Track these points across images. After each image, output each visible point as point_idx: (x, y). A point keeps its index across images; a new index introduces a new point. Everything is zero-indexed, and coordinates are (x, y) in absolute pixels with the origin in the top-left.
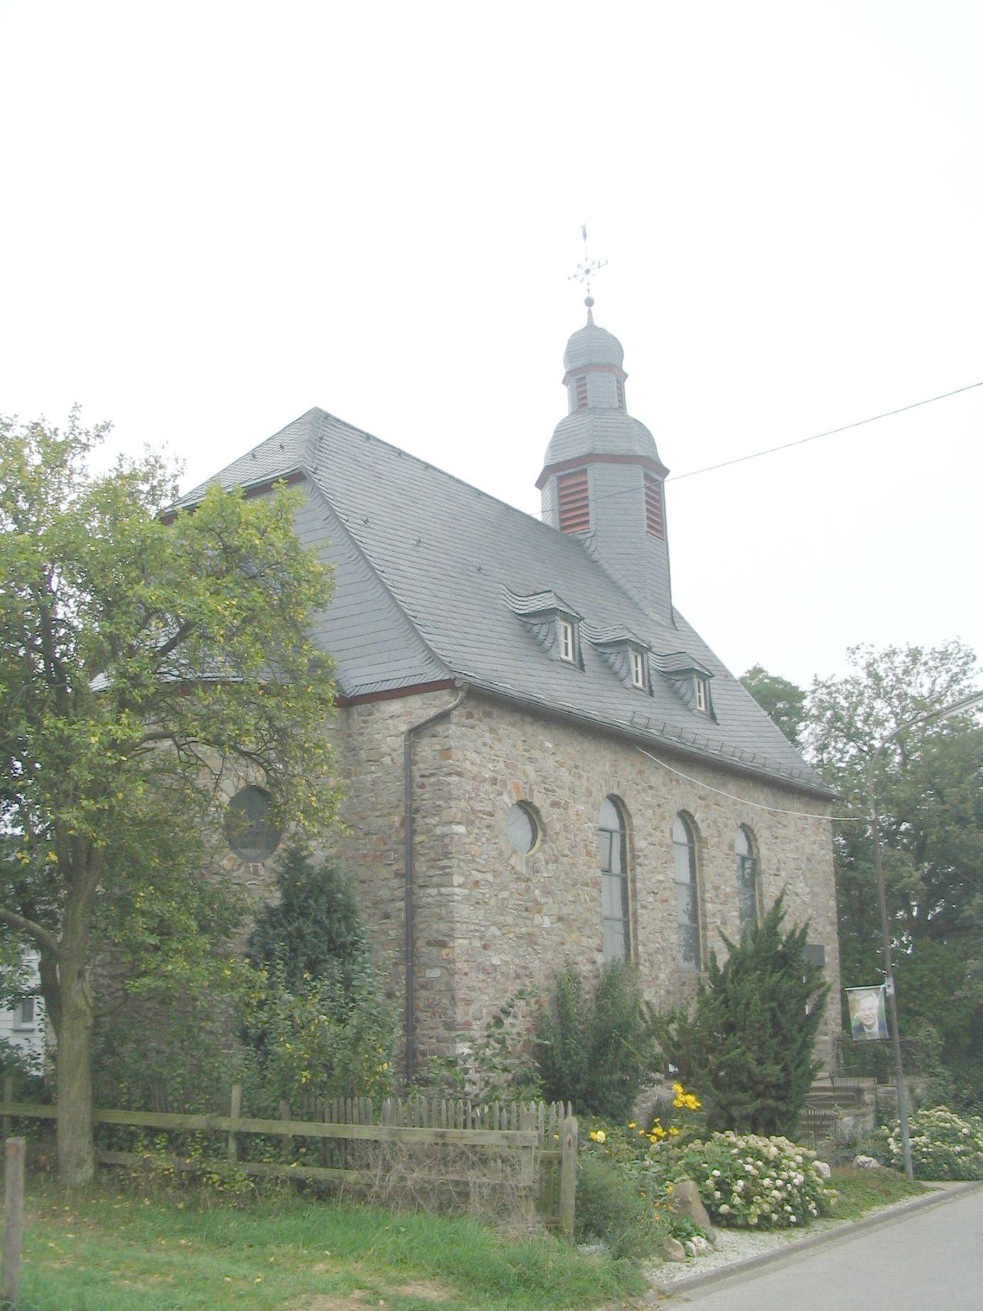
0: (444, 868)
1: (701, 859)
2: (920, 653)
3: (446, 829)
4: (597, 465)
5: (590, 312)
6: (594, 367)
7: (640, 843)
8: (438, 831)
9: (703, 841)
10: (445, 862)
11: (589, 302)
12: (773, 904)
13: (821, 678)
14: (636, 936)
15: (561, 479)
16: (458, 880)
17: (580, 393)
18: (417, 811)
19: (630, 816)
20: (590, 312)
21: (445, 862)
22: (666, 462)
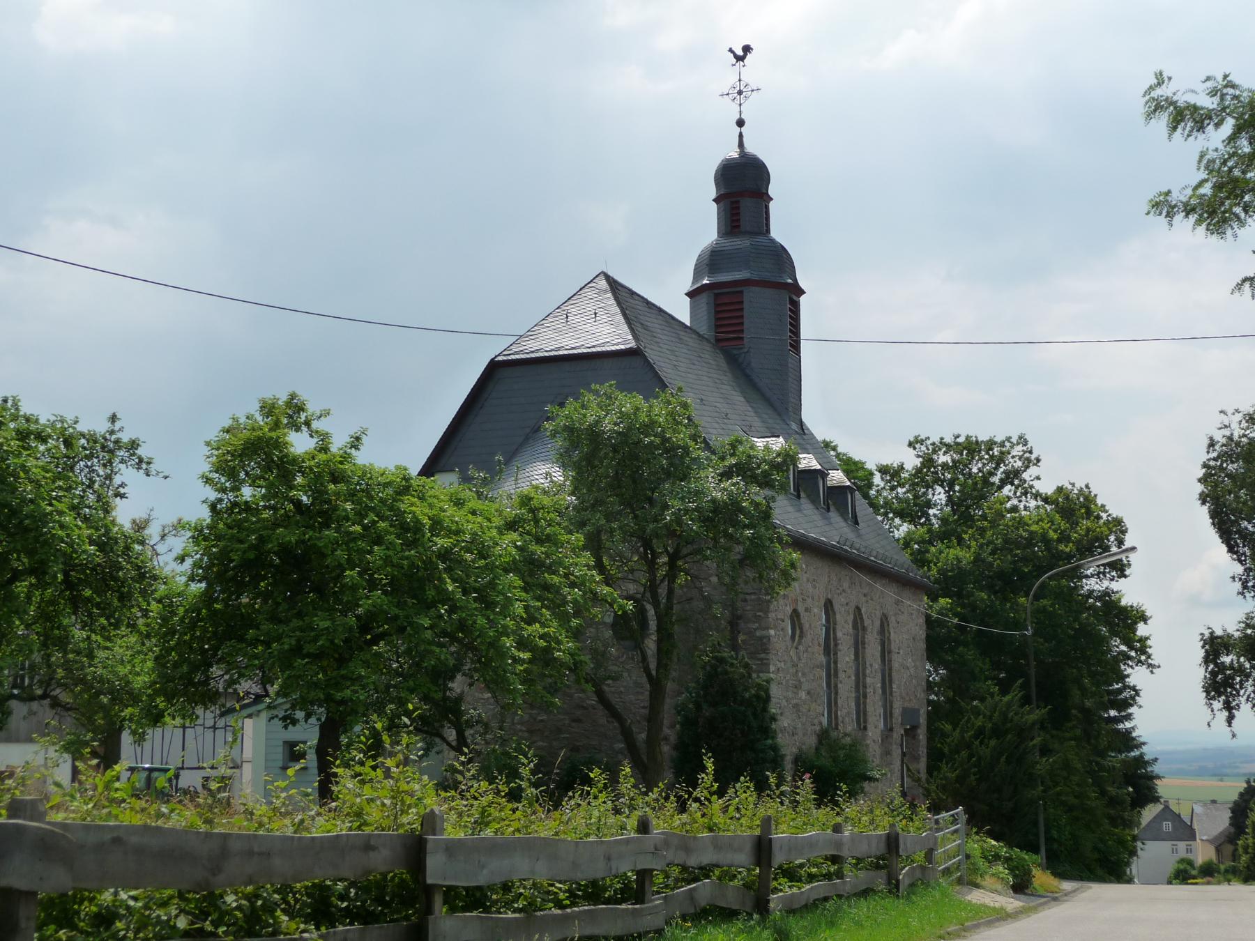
0: (762, 659)
1: (863, 643)
2: (1122, 575)
3: (764, 633)
4: (753, 288)
5: (741, 136)
6: (742, 187)
7: (839, 634)
8: (758, 634)
9: (864, 629)
10: (763, 656)
11: (740, 123)
12: (208, 487)
13: (1149, 643)
14: (836, 703)
15: (717, 295)
16: (772, 668)
17: (733, 209)
18: (739, 617)
19: (834, 614)
20: (741, 136)
21: (763, 656)
22: (802, 283)
